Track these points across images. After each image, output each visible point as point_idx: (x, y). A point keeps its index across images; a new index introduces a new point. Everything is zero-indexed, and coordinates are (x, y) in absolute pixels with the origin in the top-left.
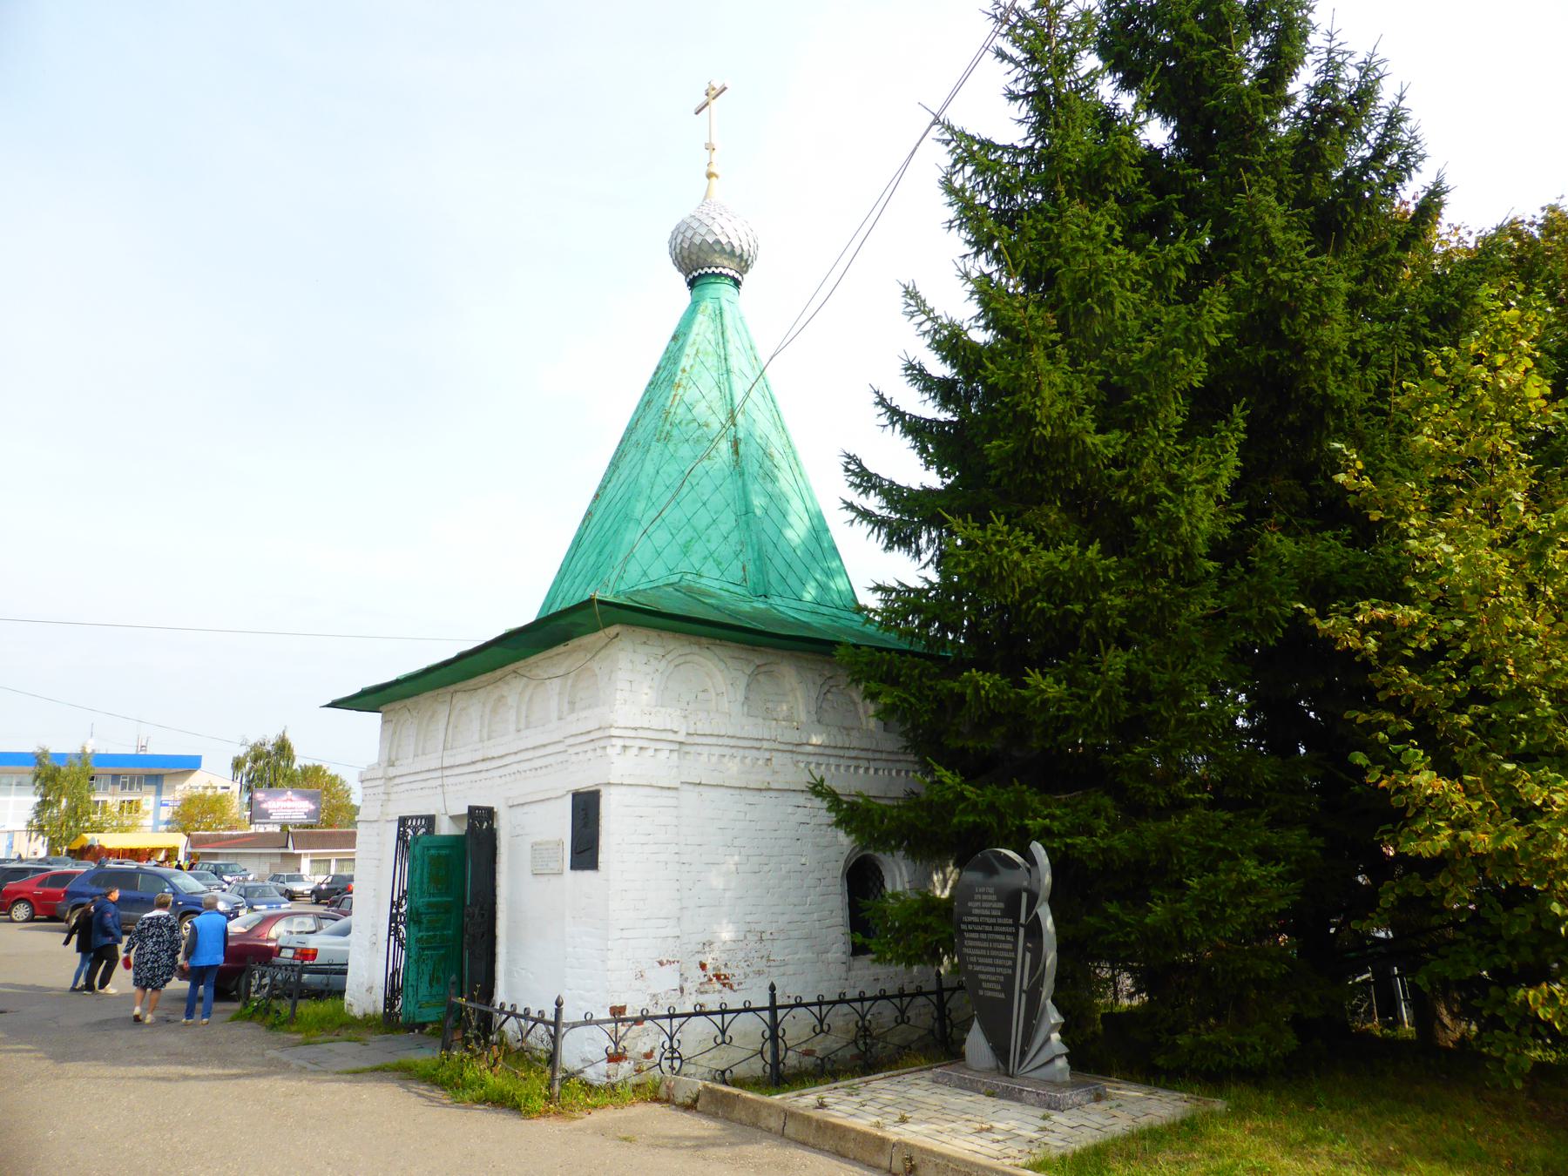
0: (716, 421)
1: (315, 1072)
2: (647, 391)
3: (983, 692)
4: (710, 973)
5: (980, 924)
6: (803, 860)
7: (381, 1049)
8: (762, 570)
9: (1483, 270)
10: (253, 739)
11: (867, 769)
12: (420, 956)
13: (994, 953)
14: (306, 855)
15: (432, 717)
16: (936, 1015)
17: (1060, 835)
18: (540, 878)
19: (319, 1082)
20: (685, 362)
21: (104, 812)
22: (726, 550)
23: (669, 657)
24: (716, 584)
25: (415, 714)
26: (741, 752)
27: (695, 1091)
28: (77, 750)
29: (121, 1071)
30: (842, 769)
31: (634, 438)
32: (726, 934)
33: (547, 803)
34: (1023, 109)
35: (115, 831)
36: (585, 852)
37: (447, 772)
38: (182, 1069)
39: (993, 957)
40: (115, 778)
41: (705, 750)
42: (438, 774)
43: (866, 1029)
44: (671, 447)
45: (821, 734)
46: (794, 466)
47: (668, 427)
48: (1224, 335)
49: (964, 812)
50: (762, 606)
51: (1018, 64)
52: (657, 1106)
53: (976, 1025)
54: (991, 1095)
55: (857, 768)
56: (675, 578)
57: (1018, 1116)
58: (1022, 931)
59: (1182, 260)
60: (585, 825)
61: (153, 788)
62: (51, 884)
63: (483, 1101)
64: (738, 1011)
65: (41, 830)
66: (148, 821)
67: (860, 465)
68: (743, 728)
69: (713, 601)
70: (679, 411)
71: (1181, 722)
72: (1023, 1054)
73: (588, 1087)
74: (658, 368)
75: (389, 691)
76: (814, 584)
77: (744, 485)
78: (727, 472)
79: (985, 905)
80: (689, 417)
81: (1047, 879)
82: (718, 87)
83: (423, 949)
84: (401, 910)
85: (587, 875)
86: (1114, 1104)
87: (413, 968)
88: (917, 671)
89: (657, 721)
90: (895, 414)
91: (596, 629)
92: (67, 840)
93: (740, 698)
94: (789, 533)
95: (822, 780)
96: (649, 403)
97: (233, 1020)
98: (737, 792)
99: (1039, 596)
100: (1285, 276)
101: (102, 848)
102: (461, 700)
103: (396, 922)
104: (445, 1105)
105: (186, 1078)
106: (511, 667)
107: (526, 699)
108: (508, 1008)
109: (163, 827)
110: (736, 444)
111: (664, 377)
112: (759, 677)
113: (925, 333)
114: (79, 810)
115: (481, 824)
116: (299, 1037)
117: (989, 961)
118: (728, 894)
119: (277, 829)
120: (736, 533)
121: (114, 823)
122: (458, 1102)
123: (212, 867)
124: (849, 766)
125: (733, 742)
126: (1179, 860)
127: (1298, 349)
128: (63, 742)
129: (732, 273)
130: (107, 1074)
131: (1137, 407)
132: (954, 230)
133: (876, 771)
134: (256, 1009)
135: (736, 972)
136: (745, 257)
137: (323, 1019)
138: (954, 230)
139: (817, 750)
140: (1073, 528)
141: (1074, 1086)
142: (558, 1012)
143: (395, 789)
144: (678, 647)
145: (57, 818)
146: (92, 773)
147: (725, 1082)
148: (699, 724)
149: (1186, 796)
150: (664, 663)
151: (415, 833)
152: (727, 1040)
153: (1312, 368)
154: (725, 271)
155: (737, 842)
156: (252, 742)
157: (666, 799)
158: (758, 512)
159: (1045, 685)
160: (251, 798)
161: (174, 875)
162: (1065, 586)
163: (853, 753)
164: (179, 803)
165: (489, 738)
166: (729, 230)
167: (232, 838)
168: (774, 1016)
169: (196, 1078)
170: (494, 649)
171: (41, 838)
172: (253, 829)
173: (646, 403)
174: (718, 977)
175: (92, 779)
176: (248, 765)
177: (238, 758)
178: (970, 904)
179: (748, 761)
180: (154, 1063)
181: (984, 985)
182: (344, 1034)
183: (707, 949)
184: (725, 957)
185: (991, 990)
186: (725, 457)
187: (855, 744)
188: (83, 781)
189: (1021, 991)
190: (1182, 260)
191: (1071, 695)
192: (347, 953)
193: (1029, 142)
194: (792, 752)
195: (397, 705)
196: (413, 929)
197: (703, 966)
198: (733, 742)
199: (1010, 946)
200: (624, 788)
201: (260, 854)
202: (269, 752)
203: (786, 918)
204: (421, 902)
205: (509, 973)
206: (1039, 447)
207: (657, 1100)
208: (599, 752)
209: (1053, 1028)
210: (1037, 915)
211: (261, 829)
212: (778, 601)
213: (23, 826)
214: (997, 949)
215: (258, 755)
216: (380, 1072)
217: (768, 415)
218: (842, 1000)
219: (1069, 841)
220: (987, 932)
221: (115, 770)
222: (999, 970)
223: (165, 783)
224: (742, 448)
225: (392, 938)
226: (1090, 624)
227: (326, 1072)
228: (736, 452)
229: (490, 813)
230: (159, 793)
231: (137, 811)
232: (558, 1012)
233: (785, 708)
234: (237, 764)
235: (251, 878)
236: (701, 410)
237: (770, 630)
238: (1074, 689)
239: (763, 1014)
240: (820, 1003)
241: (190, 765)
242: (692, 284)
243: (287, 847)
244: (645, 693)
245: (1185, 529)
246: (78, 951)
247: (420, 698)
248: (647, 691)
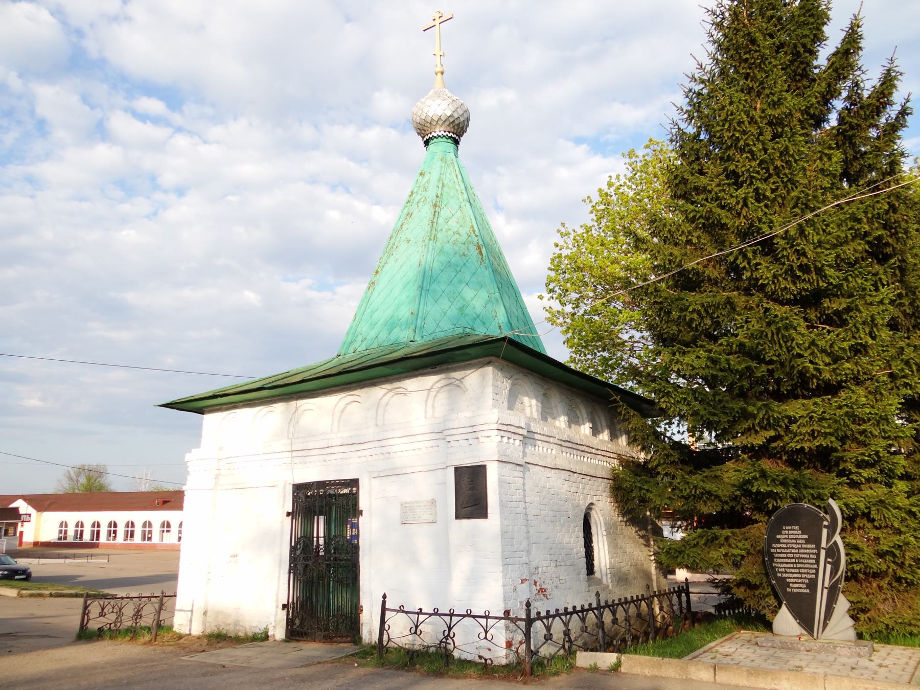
13: (799, 566)
39: (799, 568)
58: (823, 553)
117: (797, 571)
178: (778, 537)
181: (805, 586)
185: (798, 587)
194: (561, 445)
214: (802, 563)
218: (436, 613)
220: (794, 553)
225: (292, 575)
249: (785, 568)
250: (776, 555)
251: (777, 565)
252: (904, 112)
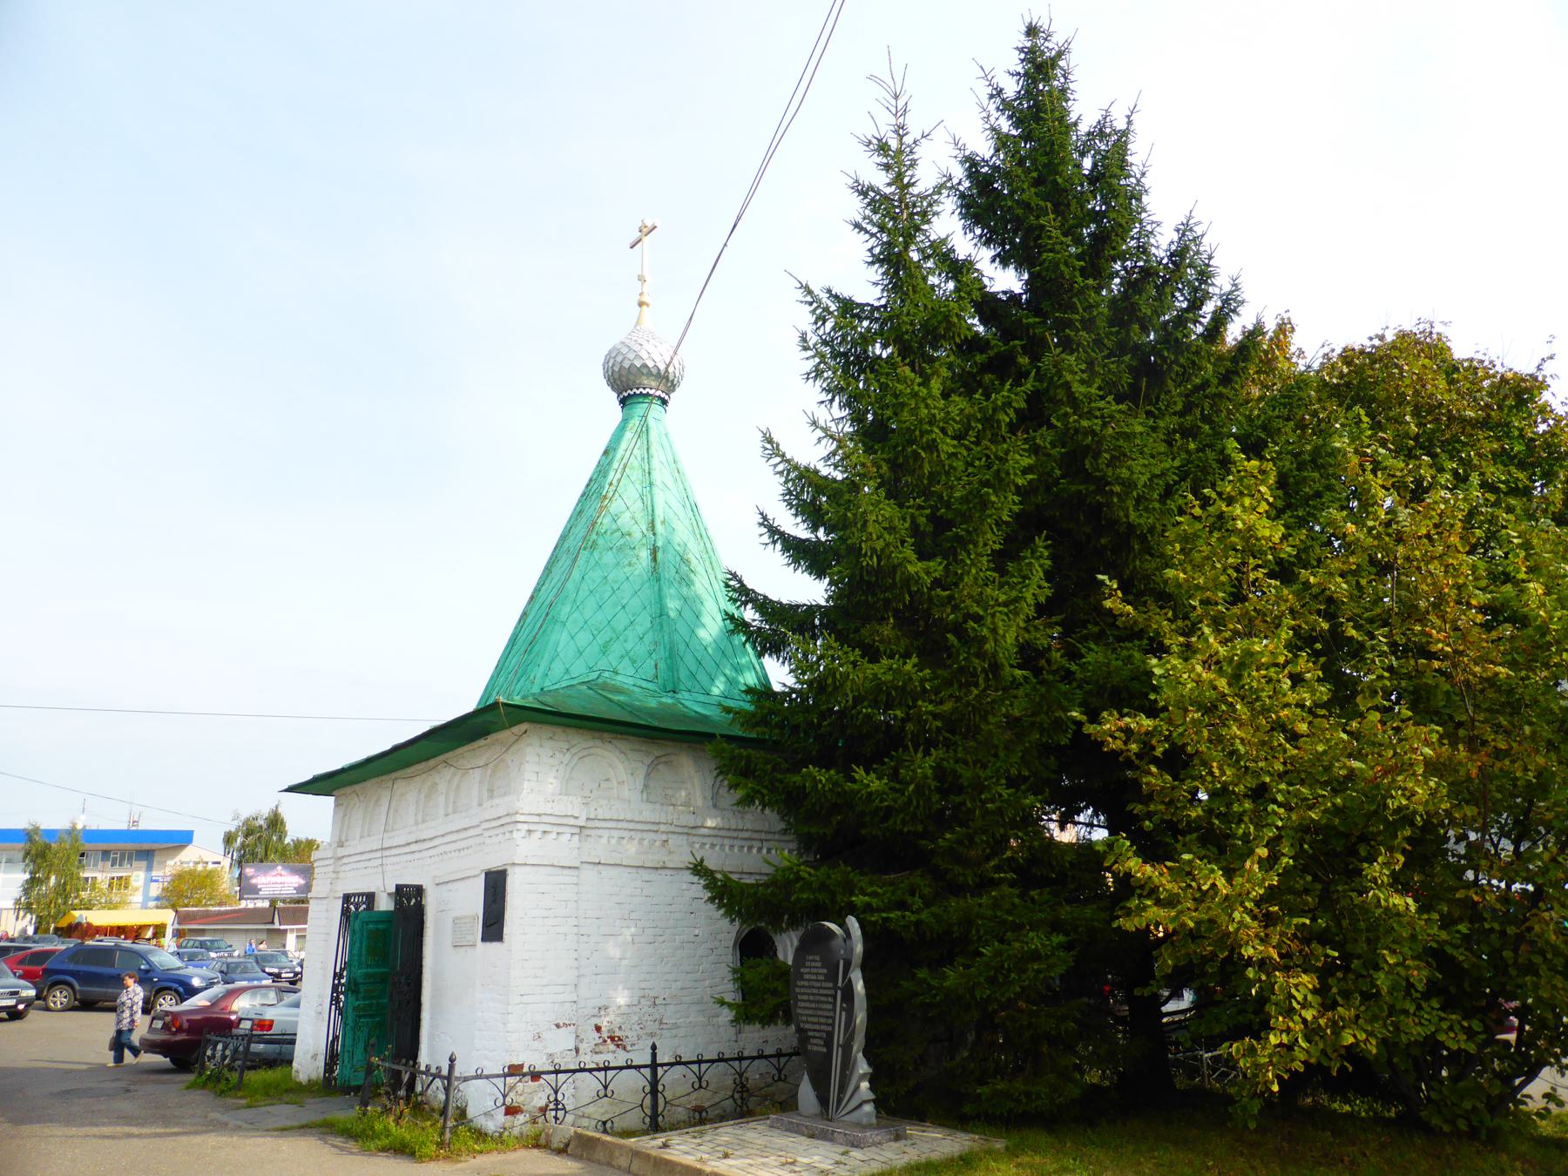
0: (638, 530)
1: (248, 1130)
2: (579, 501)
3: (820, 786)
4: (605, 1035)
5: (809, 987)
6: (697, 932)
7: (314, 1110)
8: (672, 667)
9: (1290, 404)
10: (245, 814)
11: (760, 849)
12: (356, 1022)
13: (820, 1013)
14: (292, 930)
15: (377, 801)
17: (880, 910)
18: (458, 949)
19: (246, 1137)
20: (612, 476)
21: (93, 888)
22: (641, 650)
23: (573, 751)
24: (630, 681)
25: (362, 798)
26: (639, 835)
27: (568, 1136)
28: (66, 825)
29: (73, 1131)
30: (736, 849)
31: (566, 545)
32: (622, 999)
33: (467, 882)
34: (876, 273)
35: (103, 908)
36: (493, 927)
37: (386, 853)
38: (127, 1129)
40: (106, 854)
41: (605, 834)
42: (379, 854)
43: (743, 1086)
44: (596, 554)
45: (716, 817)
46: (710, 570)
47: (594, 536)
48: (1030, 477)
49: (802, 890)
50: (670, 701)
51: (873, 235)
52: (535, 1151)
54: (812, 1136)
55: (750, 848)
56: (594, 676)
57: (823, 1152)
58: (839, 992)
59: (1008, 404)
60: (494, 901)
61: (144, 864)
62: (30, 963)
63: (384, 1149)
65: (28, 908)
66: (138, 898)
67: (740, 581)
68: (641, 812)
69: (622, 698)
70: (605, 521)
71: (986, 812)
72: (839, 1101)
73: (480, 1135)
74: (590, 480)
75: (335, 779)
76: (723, 679)
77: (660, 590)
78: (646, 578)
80: (614, 527)
81: (859, 948)
82: (649, 224)
83: (360, 1017)
84: (343, 981)
85: (493, 946)
86: (909, 1142)
87: (350, 1034)
88: (769, 767)
89: (558, 809)
90: (774, 532)
91: (503, 728)
92: (55, 918)
93: (640, 786)
94: (701, 633)
95: (702, 860)
96: (581, 512)
97: (188, 1088)
98: (634, 870)
99: (866, 703)
100: (1085, 423)
101: (89, 925)
102: (400, 786)
104: (352, 1153)
105: (129, 1136)
106: (442, 758)
107: (454, 786)
108: (433, 1070)
109: (152, 904)
110: (654, 552)
111: (595, 492)
112: (660, 767)
113: (781, 473)
114: (68, 887)
115: (410, 902)
116: (244, 1102)
117: (815, 1020)
118: (624, 962)
119: (266, 904)
120: (651, 633)
121: (103, 900)
122: (365, 1151)
123: (197, 944)
124: (743, 847)
125: (631, 826)
126: (978, 931)
127: (1102, 483)
128: (53, 818)
129: (659, 393)
130: (59, 1133)
131: (958, 538)
132: (811, 381)
133: (769, 851)
134: (210, 1077)
135: (630, 1034)
136: (671, 378)
137: (269, 1085)
138: (811, 381)
139: (712, 832)
140: (904, 642)
141: (878, 1127)
142: (451, 1067)
143: (343, 868)
145: (45, 896)
146: (82, 849)
147: (605, 1132)
148: (600, 811)
149: (992, 875)
150: (568, 755)
151: (357, 909)
152: (609, 1094)
153: (1115, 500)
155: (633, 916)
156: (243, 818)
157: (568, 877)
158: (672, 614)
159: (871, 782)
160: (240, 874)
161: (150, 952)
162: (889, 694)
163: (747, 835)
164: (169, 879)
165: (424, 821)
166: (655, 355)
167: (219, 913)
168: (654, 1073)
169: (139, 1136)
170: (423, 742)
171: (29, 916)
172: (243, 904)
173: (578, 513)
174: (612, 1039)
175: (82, 855)
176: (239, 840)
177: (230, 833)
179: (646, 842)
180: (104, 1124)
182: (286, 1098)
183: (603, 1013)
184: (619, 1020)
186: (644, 564)
187: (748, 826)
188: (73, 857)
189: (838, 1045)
190: (1008, 404)
191: (891, 789)
192: (297, 1022)
193: (883, 302)
195: (348, 790)
196: (351, 998)
197: (598, 1029)
198: (631, 826)
199: (830, 1007)
200: (527, 868)
201: (247, 930)
202: (261, 827)
203: (679, 984)
204: (359, 973)
205: (431, 1037)
206: (868, 573)
207: (537, 1146)
208: (508, 835)
209: (862, 1078)
210: (850, 980)
211: (251, 905)
212: (686, 695)
213: (10, 904)
215: (249, 830)
216: (305, 1128)
217: (687, 523)
219: (884, 915)
221: (104, 846)
222: (823, 1027)
223: (156, 859)
224: (660, 555)
226: (910, 727)
227: (258, 1130)
228: (654, 559)
229: (419, 891)
230: (149, 868)
231: (126, 888)
232: (451, 1067)
233: (683, 794)
234: (229, 839)
235: (236, 954)
236: (625, 520)
237: (662, 726)
238: (892, 784)
241: (181, 840)
242: (623, 402)
243: (273, 923)
244: (551, 784)
245: (989, 646)
246: (111, 1049)
247: (368, 784)
248: (552, 780)
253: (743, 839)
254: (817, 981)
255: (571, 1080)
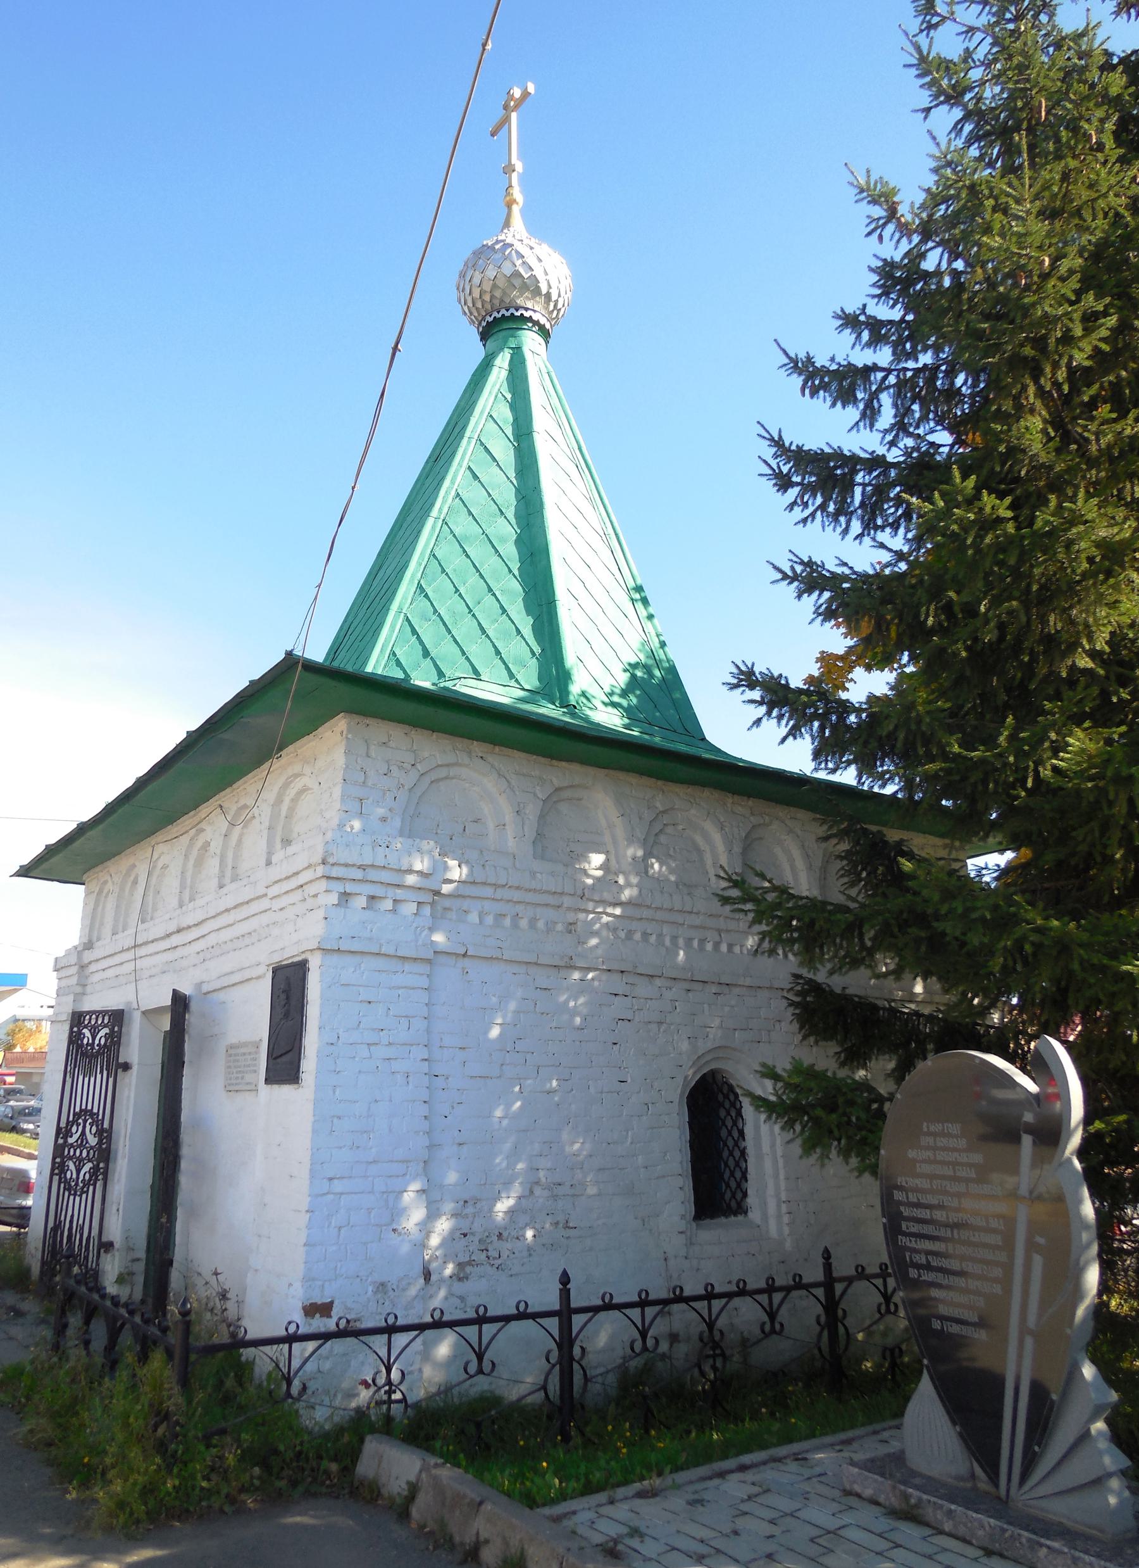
16: (823, 1319)
42: (129, 955)
43: (716, 1345)
53: (926, 1378)
60: (286, 1015)
64: (507, 1319)
79: (941, 1156)
84: (71, 1140)
98: (521, 969)
103: (62, 1156)
129: (543, 321)
144: (415, 723)
154: (536, 317)
157: (413, 976)
163: (698, 921)
165: (192, 899)
178: (911, 1154)
189: (1023, 1331)
198: (517, 895)
225: (56, 1178)
239: (815, 1291)
240: (643, 1303)
249: (928, 1253)
250: (906, 1212)
251: (912, 1243)
252: (803, 394)
253: (692, 927)
254: (955, 1179)
255: (419, 1340)
